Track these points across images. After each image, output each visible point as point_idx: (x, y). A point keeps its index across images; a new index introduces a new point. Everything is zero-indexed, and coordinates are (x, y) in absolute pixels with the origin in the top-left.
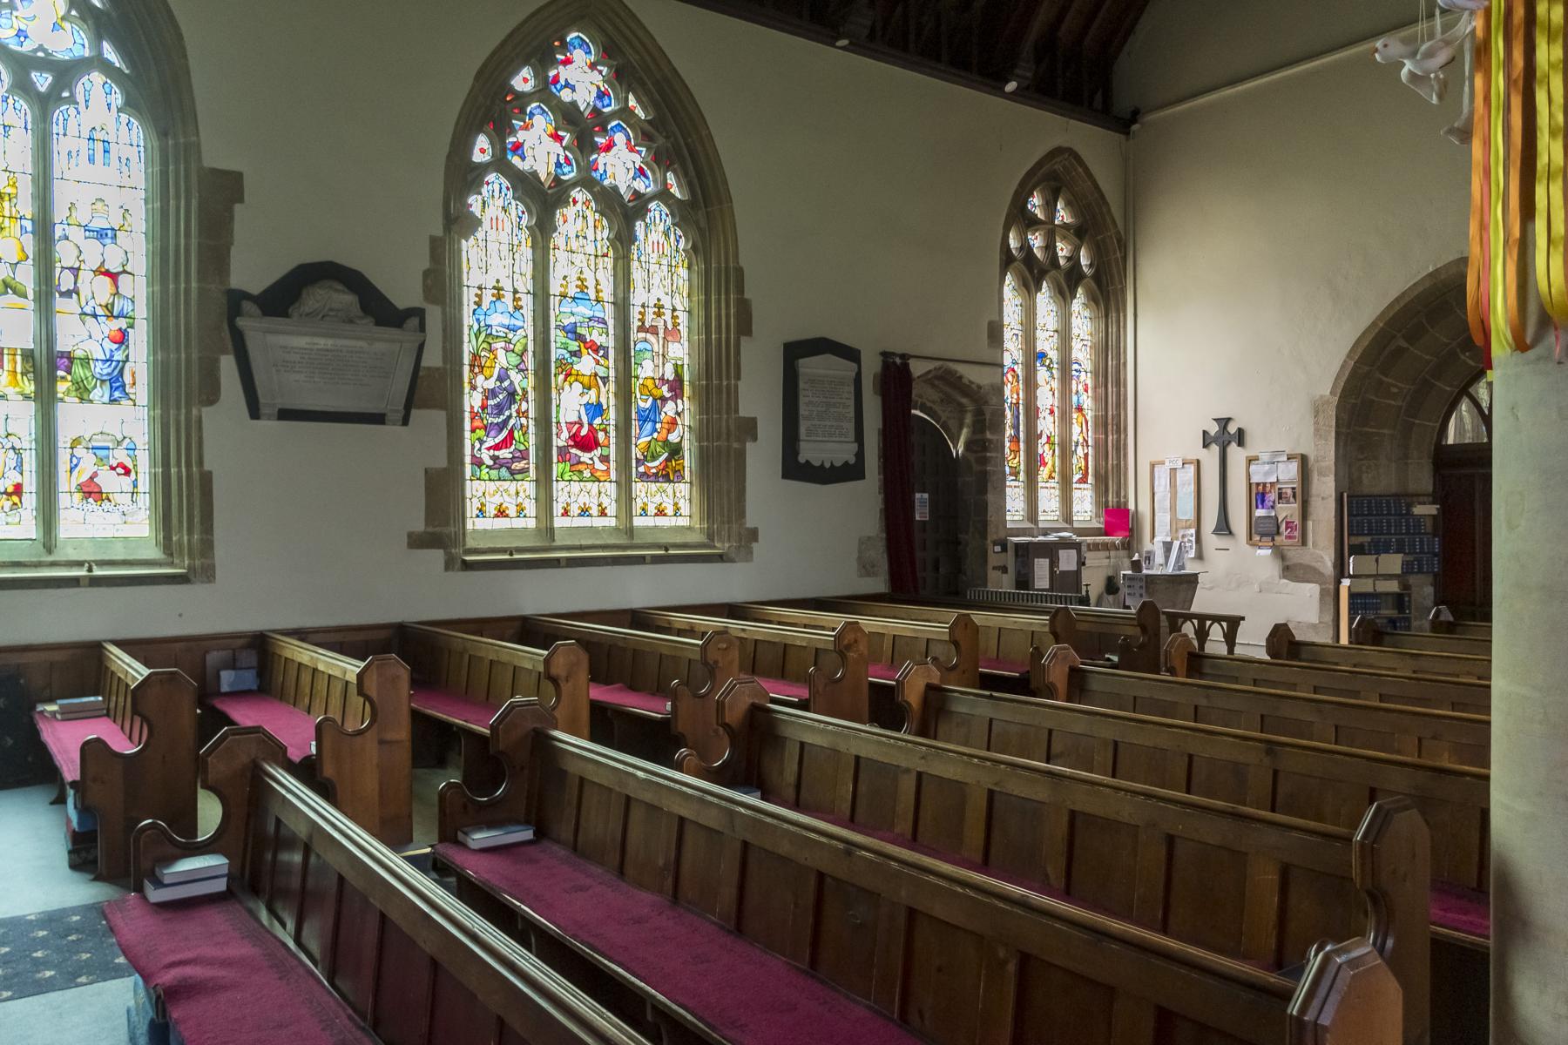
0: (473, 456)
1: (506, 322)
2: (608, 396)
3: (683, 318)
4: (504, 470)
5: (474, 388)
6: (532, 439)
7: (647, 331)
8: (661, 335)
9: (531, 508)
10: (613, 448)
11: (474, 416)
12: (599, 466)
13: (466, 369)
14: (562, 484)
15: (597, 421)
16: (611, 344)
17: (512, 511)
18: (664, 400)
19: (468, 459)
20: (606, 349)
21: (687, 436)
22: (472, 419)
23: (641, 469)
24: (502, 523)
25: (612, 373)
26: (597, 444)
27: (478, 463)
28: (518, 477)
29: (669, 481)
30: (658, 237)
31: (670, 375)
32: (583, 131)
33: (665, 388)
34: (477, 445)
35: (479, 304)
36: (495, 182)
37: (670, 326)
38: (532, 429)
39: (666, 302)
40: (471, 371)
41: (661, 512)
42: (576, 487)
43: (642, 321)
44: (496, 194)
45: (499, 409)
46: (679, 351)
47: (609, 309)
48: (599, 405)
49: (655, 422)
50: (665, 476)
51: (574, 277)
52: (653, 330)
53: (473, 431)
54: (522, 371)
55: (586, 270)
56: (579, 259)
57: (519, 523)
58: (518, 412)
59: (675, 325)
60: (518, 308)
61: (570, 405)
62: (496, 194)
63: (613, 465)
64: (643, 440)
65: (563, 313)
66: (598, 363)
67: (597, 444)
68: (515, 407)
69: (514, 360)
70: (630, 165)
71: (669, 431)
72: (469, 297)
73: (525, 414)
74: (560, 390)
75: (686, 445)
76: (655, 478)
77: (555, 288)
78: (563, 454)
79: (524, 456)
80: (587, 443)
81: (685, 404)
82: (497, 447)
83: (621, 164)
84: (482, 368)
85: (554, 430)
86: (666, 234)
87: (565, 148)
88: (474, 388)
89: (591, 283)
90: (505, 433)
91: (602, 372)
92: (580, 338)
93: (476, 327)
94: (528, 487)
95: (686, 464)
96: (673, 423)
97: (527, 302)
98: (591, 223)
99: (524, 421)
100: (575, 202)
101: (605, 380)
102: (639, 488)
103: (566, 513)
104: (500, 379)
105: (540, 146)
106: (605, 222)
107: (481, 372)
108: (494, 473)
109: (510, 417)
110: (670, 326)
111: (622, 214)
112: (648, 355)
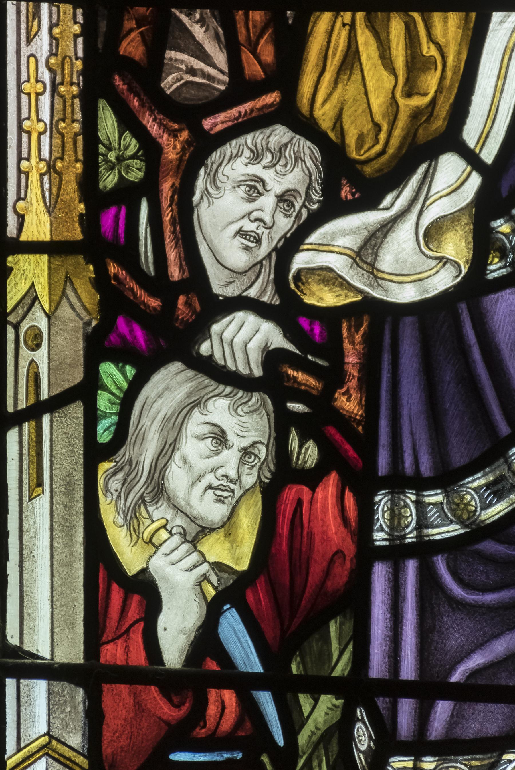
107: (268, 92)
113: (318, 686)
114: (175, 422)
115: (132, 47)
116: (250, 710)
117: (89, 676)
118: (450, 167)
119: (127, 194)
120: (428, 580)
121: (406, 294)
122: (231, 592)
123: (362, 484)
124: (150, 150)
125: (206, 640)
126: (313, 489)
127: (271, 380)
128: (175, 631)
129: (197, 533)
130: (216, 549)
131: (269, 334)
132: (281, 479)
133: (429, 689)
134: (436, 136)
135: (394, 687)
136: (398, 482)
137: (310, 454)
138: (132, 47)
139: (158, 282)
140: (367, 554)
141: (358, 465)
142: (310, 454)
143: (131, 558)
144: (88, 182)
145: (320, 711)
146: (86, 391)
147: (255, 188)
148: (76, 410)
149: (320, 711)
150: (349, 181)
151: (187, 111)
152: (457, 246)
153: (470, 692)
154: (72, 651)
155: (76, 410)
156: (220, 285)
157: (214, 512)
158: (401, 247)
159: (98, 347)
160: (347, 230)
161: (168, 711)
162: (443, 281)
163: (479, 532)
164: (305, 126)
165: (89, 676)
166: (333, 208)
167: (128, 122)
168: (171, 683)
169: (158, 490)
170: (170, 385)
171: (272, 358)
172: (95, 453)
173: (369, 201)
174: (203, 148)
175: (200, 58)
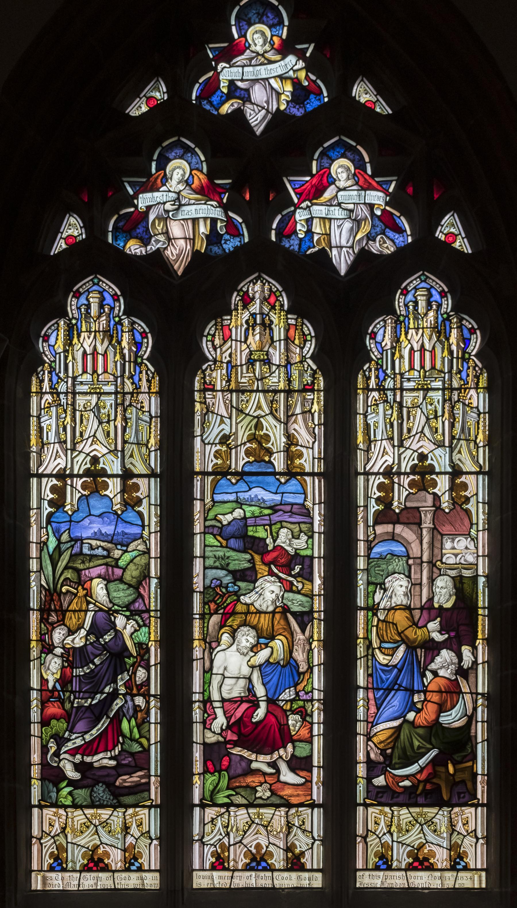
0: (44, 764)
1: (108, 529)
2: (311, 651)
3: (477, 487)
4: (100, 789)
5: (48, 648)
6: (155, 733)
7: (396, 520)
8: (427, 522)
9: (151, 856)
10: (318, 744)
11: (47, 696)
12: (288, 776)
13: (34, 617)
14: (210, 812)
15: (288, 695)
16: (318, 548)
17: (116, 858)
18: (432, 648)
19: (35, 771)
20: (307, 562)
21: (481, 714)
22: (43, 703)
23: (380, 781)
24: (90, 881)
25: (318, 604)
26: (285, 737)
27: (53, 776)
28: (128, 800)
29: (440, 804)
30: (419, 340)
31: (444, 594)
32: (257, 167)
33: (433, 625)
34: (53, 747)
35: (58, 504)
36: (95, 299)
37: (445, 504)
38: (154, 715)
39: (440, 460)
40: (43, 620)
41: (420, 862)
42: (241, 816)
43: (386, 502)
44: (94, 310)
45: (93, 683)
46: (468, 551)
47: (315, 488)
48: (290, 662)
49: (412, 692)
50: (429, 794)
51: (242, 435)
52: (411, 517)
53: (45, 722)
54: (132, 612)
55: (268, 423)
56: (257, 403)
57: (130, 881)
58: (127, 685)
59: (459, 501)
60: (131, 503)
61: (231, 665)
62: (94, 310)
63: (316, 775)
64: (384, 728)
65: (215, 506)
66: (289, 588)
67: (285, 737)
68: (122, 679)
69: (122, 595)
70: (363, 212)
71: (442, 708)
72: (40, 493)
73: (143, 689)
74: (211, 644)
75: (480, 731)
76: (410, 798)
77: (204, 456)
78: (214, 754)
79: (140, 761)
80: (267, 736)
81: (478, 654)
82: (89, 749)
83: (341, 213)
84: (62, 612)
85: (197, 714)
86: (440, 331)
87: (225, 208)
88: (48, 648)
89: (277, 439)
90: (103, 724)
91: (296, 602)
92: (254, 545)
93: (52, 543)
94: (147, 819)
95: (480, 766)
96: (451, 692)
97: (149, 490)
98: (279, 333)
99: (140, 701)
100: (247, 300)
101: (304, 618)
102: (371, 819)
103: (220, 863)
104: (95, 630)
105: (179, 211)
106: (309, 329)
107: (62, 622)
108: (82, 794)
109: (114, 695)
110: (445, 504)
111: (342, 308)
112: (399, 564)
113: (67, 691)
114: (183, 900)
115: (45, 616)
116: (59, 694)
117: (41, 690)
118: (83, 630)
119: (45, 634)
120: (80, 679)
121: (77, 646)
122: (57, 681)
123: (72, 668)
124: (47, 629)
125: (54, 686)
126: (268, 575)
127: (62, 656)
128: (51, 685)
129: (53, 674)
130: (55, 676)
131: (61, 650)
132: (63, 667)
133: (80, 692)
134: (81, 627)
135: (76, 692)
136: (76, 668)
137: (66, 664)
138: (45, 616)
139: (49, 645)
140: (73, 676)
141: (72, 666)
142: (66, 664)
143: (45, 677)
144: (40, 633)
145: (67, 694)
146: (40, 657)
147: (60, 633)
148: (310, 851)
149: (67, 694)
150: (71, 632)
151: (52, 624)
152: (83, 640)
153: (84, 692)
154: (39, 688)
155: (310, 851)
156: (56, 645)
157: (55, 671)
158: (77, 640)
159: (42, 652)
160: (71, 638)
161: (50, 694)
162: (82, 644)
163: (86, 674)
164: (66, 626)
165: (41, 690)
166: (69, 635)
167: (45, 625)
168: (50, 691)
169: (49, 669)
170: (50, 656)
171: (62, 653)
172: (41, 664)
173: (73, 634)
174: (54, 628)
175: (53, 618)
